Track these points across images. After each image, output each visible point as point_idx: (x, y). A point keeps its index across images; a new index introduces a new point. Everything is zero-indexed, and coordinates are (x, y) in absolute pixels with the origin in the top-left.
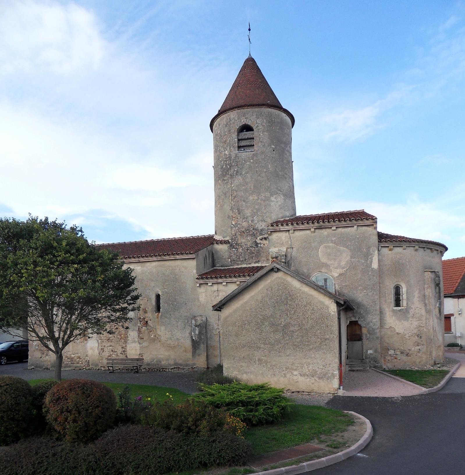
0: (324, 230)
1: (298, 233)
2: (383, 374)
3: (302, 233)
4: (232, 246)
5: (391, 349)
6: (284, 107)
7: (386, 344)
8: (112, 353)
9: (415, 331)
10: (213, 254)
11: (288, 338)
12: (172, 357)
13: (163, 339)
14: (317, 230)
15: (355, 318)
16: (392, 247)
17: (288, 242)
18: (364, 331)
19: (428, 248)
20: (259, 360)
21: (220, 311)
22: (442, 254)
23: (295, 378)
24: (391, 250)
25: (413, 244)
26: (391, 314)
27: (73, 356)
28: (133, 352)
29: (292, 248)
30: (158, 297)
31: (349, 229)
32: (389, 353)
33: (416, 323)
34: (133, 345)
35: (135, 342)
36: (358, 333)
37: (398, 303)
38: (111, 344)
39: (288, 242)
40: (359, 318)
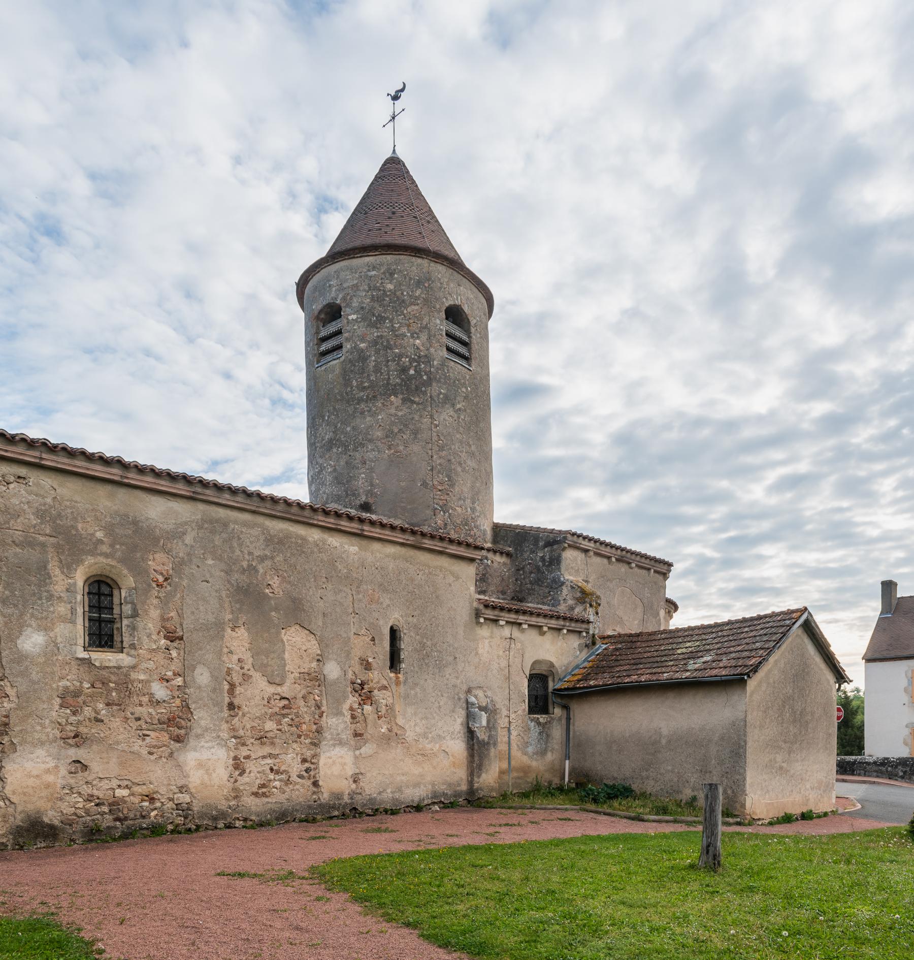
2: (879, 783)
6: (473, 266)
8: (272, 776)
10: (232, 460)
12: (428, 778)
13: (410, 735)
20: (781, 768)
22: (669, 615)
27: (120, 793)
28: (336, 770)
30: (394, 634)
34: (339, 751)
35: (341, 743)
38: (267, 750)
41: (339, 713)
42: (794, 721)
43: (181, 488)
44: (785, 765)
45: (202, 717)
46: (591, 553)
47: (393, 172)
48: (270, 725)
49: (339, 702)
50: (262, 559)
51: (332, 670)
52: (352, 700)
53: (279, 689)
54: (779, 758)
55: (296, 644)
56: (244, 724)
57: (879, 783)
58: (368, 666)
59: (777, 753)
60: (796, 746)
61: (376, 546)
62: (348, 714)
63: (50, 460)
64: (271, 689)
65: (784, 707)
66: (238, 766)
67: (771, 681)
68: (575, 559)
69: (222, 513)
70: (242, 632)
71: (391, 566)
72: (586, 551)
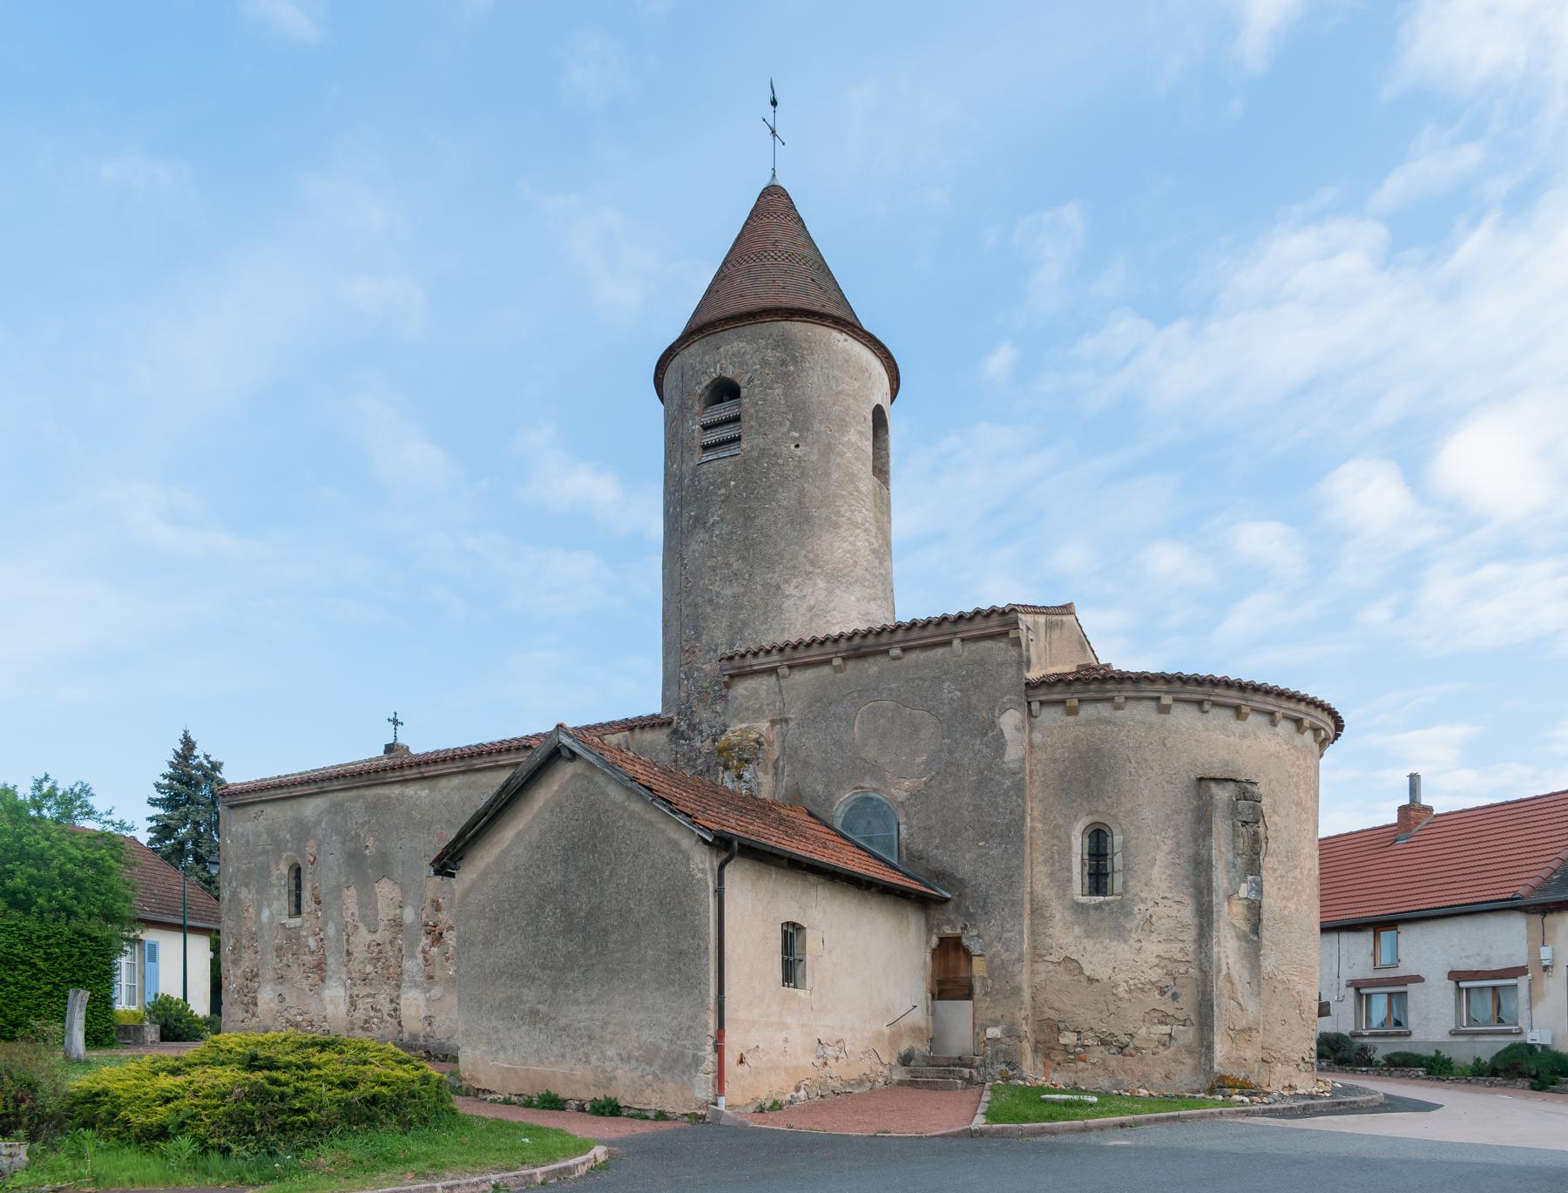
0: (871, 660)
1: (799, 677)
3: (810, 674)
4: (677, 734)
5: (1066, 1029)
7: (1051, 1014)
9: (1155, 975)
11: (594, 951)
14: (851, 664)
15: (954, 927)
16: (1075, 702)
17: (774, 703)
18: (979, 967)
19: (1215, 704)
20: (534, 1013)
21: (453, 875)
23: (608, 1066)
24: (1072, 712)
25: (1149, 690)
26: (1069, 916)
27: (299, 1018)
28: (412, 1012)
29: (787, 721)
31: (940, 651)
32: (1062, 1041)
33: (1159, 949)
35: (416, 985)
36: (963, 974)
37: (1098, 879)
38: (367, 990)
39: (774, 703)
40: (965, 928)
41: (413, 956)
42: (568, 930)
43: (313, 788)
44: (543, 1008)
45: (331, 961)
46: (784, 671)
47: (774, 205)
48: (369, 968)
49: (413, 943)
50: (363, 825)
51: (409, 915)
52: (425, 941)
53: (374, 937)
54: (529, 995)
55: (385, 891)
56: (354, 966)
57: (1183, 1119)
58: (438, 908)
59: (523, 986)
60: (570, 975)
61: (443, 782)
62: (420, 956)
63: (265, 796)
64: (370, 937)
65: (541, 907)
66: (353, 1004)
67: (510, 867)
68: (755, 692)
69: (340, 795)
70: (353, 890)
71: (456, 798)
72: (773, 671)
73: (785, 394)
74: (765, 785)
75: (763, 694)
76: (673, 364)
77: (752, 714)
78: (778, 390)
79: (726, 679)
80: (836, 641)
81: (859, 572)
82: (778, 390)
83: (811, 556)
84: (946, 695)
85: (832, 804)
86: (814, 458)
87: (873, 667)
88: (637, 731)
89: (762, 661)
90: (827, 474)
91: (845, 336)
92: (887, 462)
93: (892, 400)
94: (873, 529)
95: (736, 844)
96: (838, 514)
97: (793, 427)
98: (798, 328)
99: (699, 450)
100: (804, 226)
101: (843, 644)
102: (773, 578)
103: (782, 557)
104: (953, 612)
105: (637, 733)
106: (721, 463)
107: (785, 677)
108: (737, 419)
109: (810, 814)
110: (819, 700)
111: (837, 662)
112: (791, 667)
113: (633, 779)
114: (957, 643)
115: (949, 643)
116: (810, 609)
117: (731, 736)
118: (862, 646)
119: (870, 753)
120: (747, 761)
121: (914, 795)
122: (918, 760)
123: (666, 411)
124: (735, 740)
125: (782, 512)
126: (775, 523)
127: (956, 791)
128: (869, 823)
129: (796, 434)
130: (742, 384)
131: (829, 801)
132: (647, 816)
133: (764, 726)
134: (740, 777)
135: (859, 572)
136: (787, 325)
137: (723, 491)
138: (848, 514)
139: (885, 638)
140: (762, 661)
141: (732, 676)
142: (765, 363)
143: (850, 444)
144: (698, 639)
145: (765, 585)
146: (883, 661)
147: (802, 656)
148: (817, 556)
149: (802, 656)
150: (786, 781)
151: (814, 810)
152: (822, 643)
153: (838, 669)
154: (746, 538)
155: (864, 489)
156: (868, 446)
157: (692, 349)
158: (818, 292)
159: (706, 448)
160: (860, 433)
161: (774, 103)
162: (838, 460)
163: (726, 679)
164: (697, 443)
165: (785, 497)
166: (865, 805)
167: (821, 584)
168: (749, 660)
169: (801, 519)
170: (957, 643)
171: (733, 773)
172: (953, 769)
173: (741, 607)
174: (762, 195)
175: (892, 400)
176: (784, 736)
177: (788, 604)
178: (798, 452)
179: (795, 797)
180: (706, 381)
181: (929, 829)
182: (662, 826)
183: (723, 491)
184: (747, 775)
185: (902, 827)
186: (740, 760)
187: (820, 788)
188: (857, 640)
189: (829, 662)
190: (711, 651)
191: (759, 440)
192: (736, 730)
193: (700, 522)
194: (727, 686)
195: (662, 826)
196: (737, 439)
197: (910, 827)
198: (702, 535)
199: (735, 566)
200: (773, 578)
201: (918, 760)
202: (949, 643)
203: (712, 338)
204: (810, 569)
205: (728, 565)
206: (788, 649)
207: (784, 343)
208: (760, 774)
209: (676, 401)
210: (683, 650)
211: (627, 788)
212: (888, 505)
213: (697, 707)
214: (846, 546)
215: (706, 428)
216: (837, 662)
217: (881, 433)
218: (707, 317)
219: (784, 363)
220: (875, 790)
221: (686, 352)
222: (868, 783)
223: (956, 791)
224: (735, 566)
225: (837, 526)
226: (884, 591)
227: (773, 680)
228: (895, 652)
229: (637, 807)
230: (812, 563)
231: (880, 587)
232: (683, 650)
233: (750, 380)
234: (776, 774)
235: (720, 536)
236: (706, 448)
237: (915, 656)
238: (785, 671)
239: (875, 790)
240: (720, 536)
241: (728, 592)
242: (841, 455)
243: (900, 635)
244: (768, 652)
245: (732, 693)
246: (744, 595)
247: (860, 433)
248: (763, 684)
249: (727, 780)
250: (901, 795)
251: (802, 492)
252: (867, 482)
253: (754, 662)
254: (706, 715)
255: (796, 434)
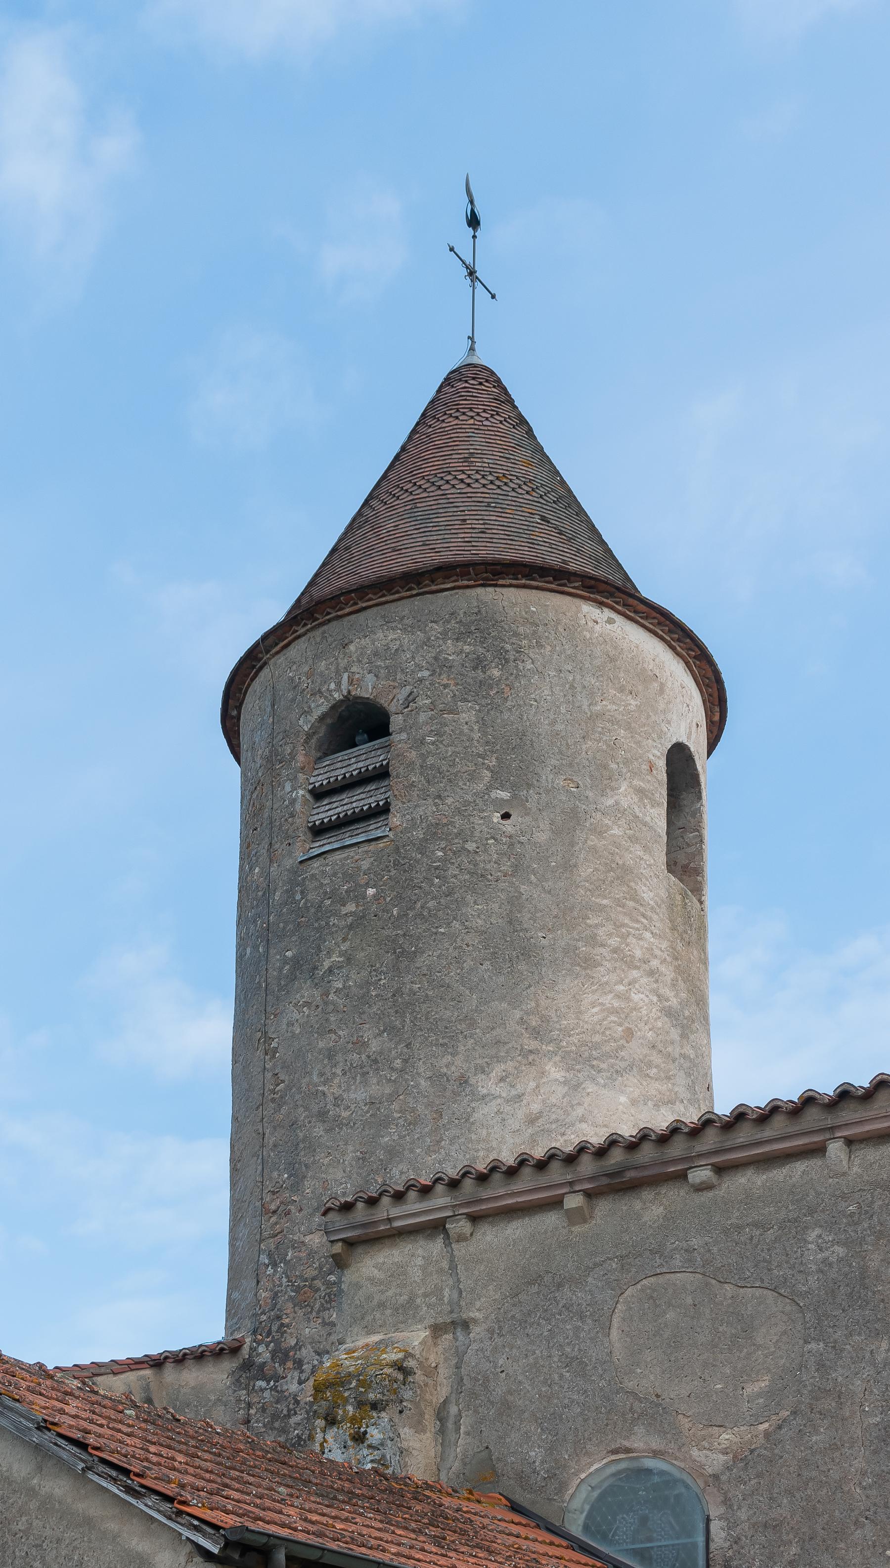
0: (647, 1194)
1: (491, 1237)
3: (516, 1230)
4: (250, 1369)
14: (603, 1206)
17: (438, 1291)
29: (465, 1325)
31: (800, 1167)
39: (438, 1291)
47: (471, 397)
72: (437, 1228)
73: (483, 723)
74: (418, 1453)
75: (416, 1274)
76: (257, 686)
77: (395, 1311)
78: (468, 715)
79: (338, 1248)
80: (571, 1159)
81: (636, 1049)
82: (468, 715)
83: (534, 1022)
84: (812, 1256)
85: (562, 1487)
86: (542, 837)
87: (652, 1208)
88: (169, 1367)
89: (414, 1210)
90: (569, 867)
91: (608, 613)
92: (700, 852)
93: (709, 753)
94: (668, 973)
95: (281, 1557)
96: (593, 940)
97: (498, 779)
98: (511, 601)
99: (303, 835)
100: (530, 432)
101: (587, 1166)
102: (454, 1065)
103: (473, 1024)
104: (827, 1088)
105: (170, 1373)
106: (354, 854)
107: (461, 1238)
108: (382, 774)
109: (515, 1508)
110: (537, 1279)
111: (573, 1201)
112: (474, 1219)
113: (44, 1426)
114: (836, 1149)
115: (819, 1150)
116: (532, 1120)
117: (344, 1359)
118: (625, 1169)
119: (647, 1379)
120: (374, 1406)
121: (742, 1459)
122: (752, 1389)
123: (244, 774)
124: (350, 1366)
125: (473, 939)
126: (458, 960)
127: (834, 1447)
128: (644, 1520)
129: (504, 795)
130: (392, 708)
131: (556, 1478)
132: (80, 1506)
133: (416, 1337)
134: (359, 1438)
135: (636, 1049)
136: (487, 594)
137: (351, 907)
138: (614, 942)
139: (678, 1148)
140: (414, 1210)
141: (350, 1244)
142: (440, 665)
143: (618, 811)
144: (296, 1187)
145: (437, 1078)
146: (673, 1194)
147: (499, 1192)
148: (545, 1019)
149: (499, 1192)
150: (463, 1444)
151: (523, 1498)
152: (541, 1165)
153: (576, 1217)
154: (398, 992)
155: (647, 895)
156: (657, 817)
157: (293, 652)
158: (555, 539)
159: (319, 831)
160: (640, 791)
161: (473, 221)
162: (593, 841)
163: (338, 1248)
164: (301, 822)
165: (481, 912)
166: (636, 1486)
167: (555, 1072)
168: (387, 1208)
169: (515, 952)
170: (836, 1149)
171: (344, 1431)
172: (829, 1404)
173: (386, 1123)
174: (448, 381)
175: (709, 753)
176: (460, 1355)
177: (483, 1112)
178: (508, 826)
179: (483, 1476)
180: (321, 706)
181: (775, 1526)
182: (112, 1526)
183: (351, 907)
184: (375, 1435)
185: (715, 1526)
186: (360, 1404)
187: (536, 1454)
188: (617, 1156)
189: (556, 1203)
190: (318, 1204)
191: (427, 809)
192: (356, 1347)
193: (303, 967)
194: (340, 1263)
195: (112, 1526)
196: (383, 811)
197: (732, 1524)
198: (307, 992)
199: (375, 1046)
200: (454, 1065)
201: (752, 1389)
202: (819, 1150)
203: (334, 628)
204: (533, 1044)
205: (360, 1045)
206: (468, 1183)
207: (481, 627)
208: (406, 1432)
209: (262, 751)
210: (265, 1211)
211: (38, 1448)
212: (702, 930)
213: (292, 1315)
214: (608, 1000)
215: (319, 794)
216: (573, 1201)
217: (686, 798)
218: (325, 590)
219: (479, 663)
220: (656, 1454)
221: (281, 659)
222: (640, 1440)
223: (834, 1447)
224: (375, 1046)
225: (589, 963)
226: (691, 1088)
227: (437, 1246)
228: (701, 1174)
229: (57, 1487)
230: (536, 1033)
231: (681, 1079)
232: (265, 1211)
233: (410, 699)
234: (442, 1431)
235: (343, 992)
236: (319, 831)
237: (743, 1180)
238: (463, 1226)
239: (656, 1454)
240: (343, 992)
241: (358, 1095)
242: (599, 831)
243: (711, 1139)
244: (426, 1191)
245: (349, 1276)
246: (391, 1098)
247: (640, 791)
248: (416, 1257)
249: (334, 1447)
250: (715, 1461)
251: (515, 901)
252: (655, 884)
253: (395, 1212)
254: (310, 1330)
255: (504, 795)
